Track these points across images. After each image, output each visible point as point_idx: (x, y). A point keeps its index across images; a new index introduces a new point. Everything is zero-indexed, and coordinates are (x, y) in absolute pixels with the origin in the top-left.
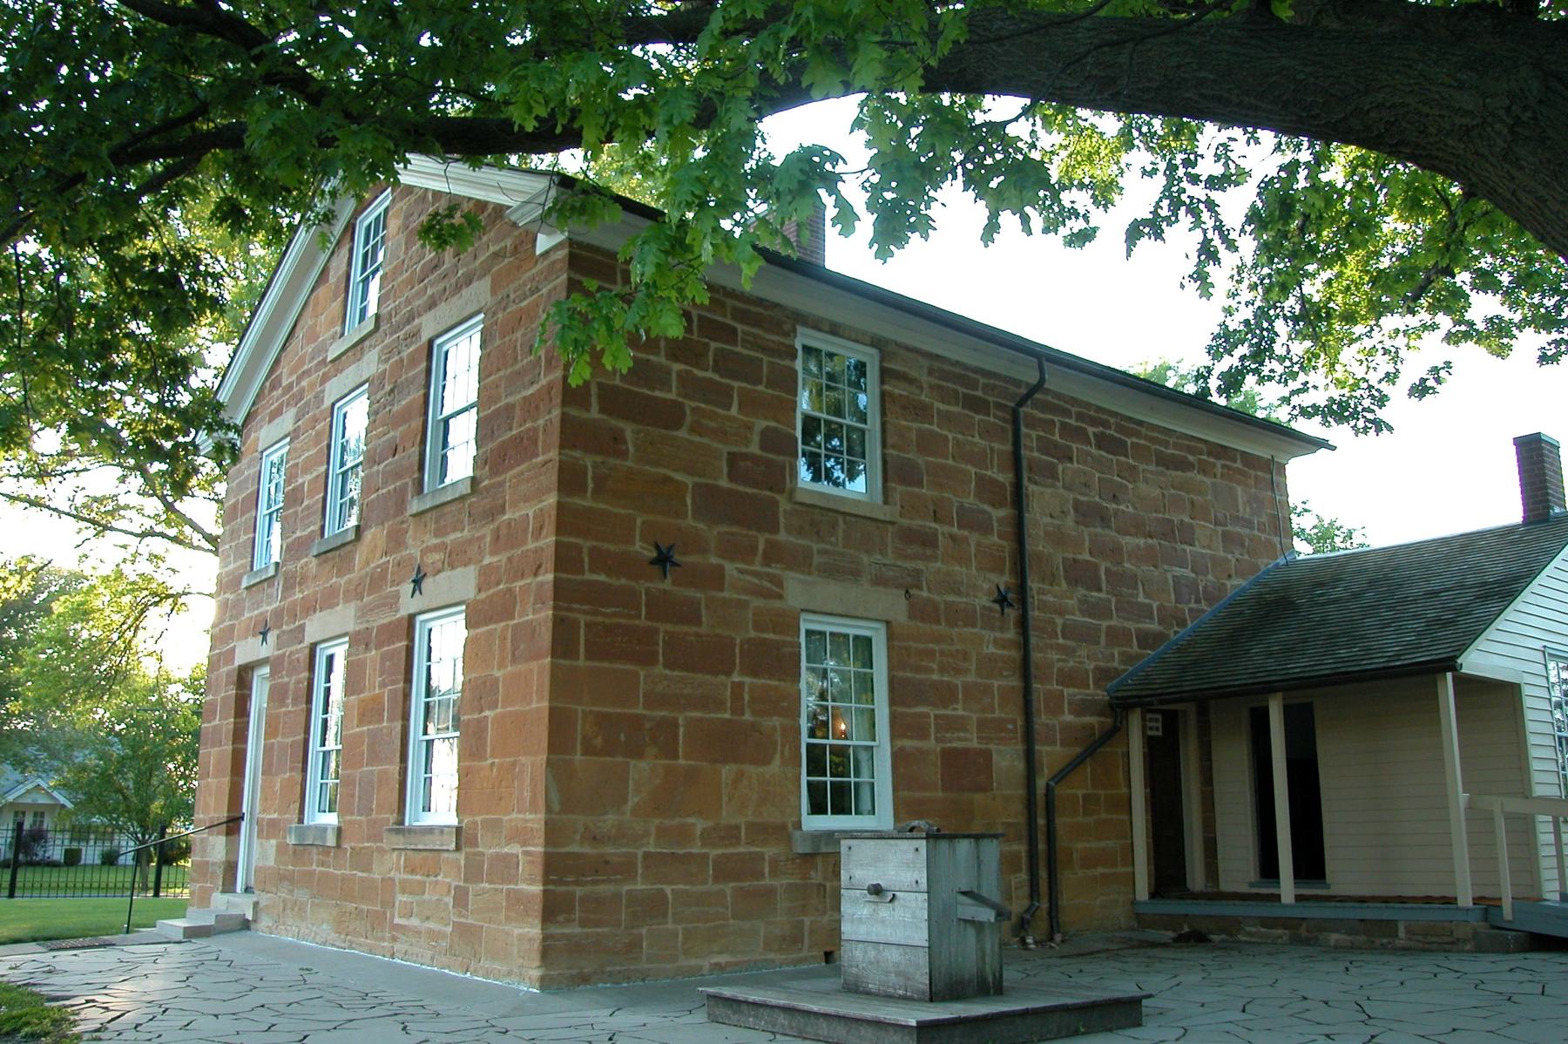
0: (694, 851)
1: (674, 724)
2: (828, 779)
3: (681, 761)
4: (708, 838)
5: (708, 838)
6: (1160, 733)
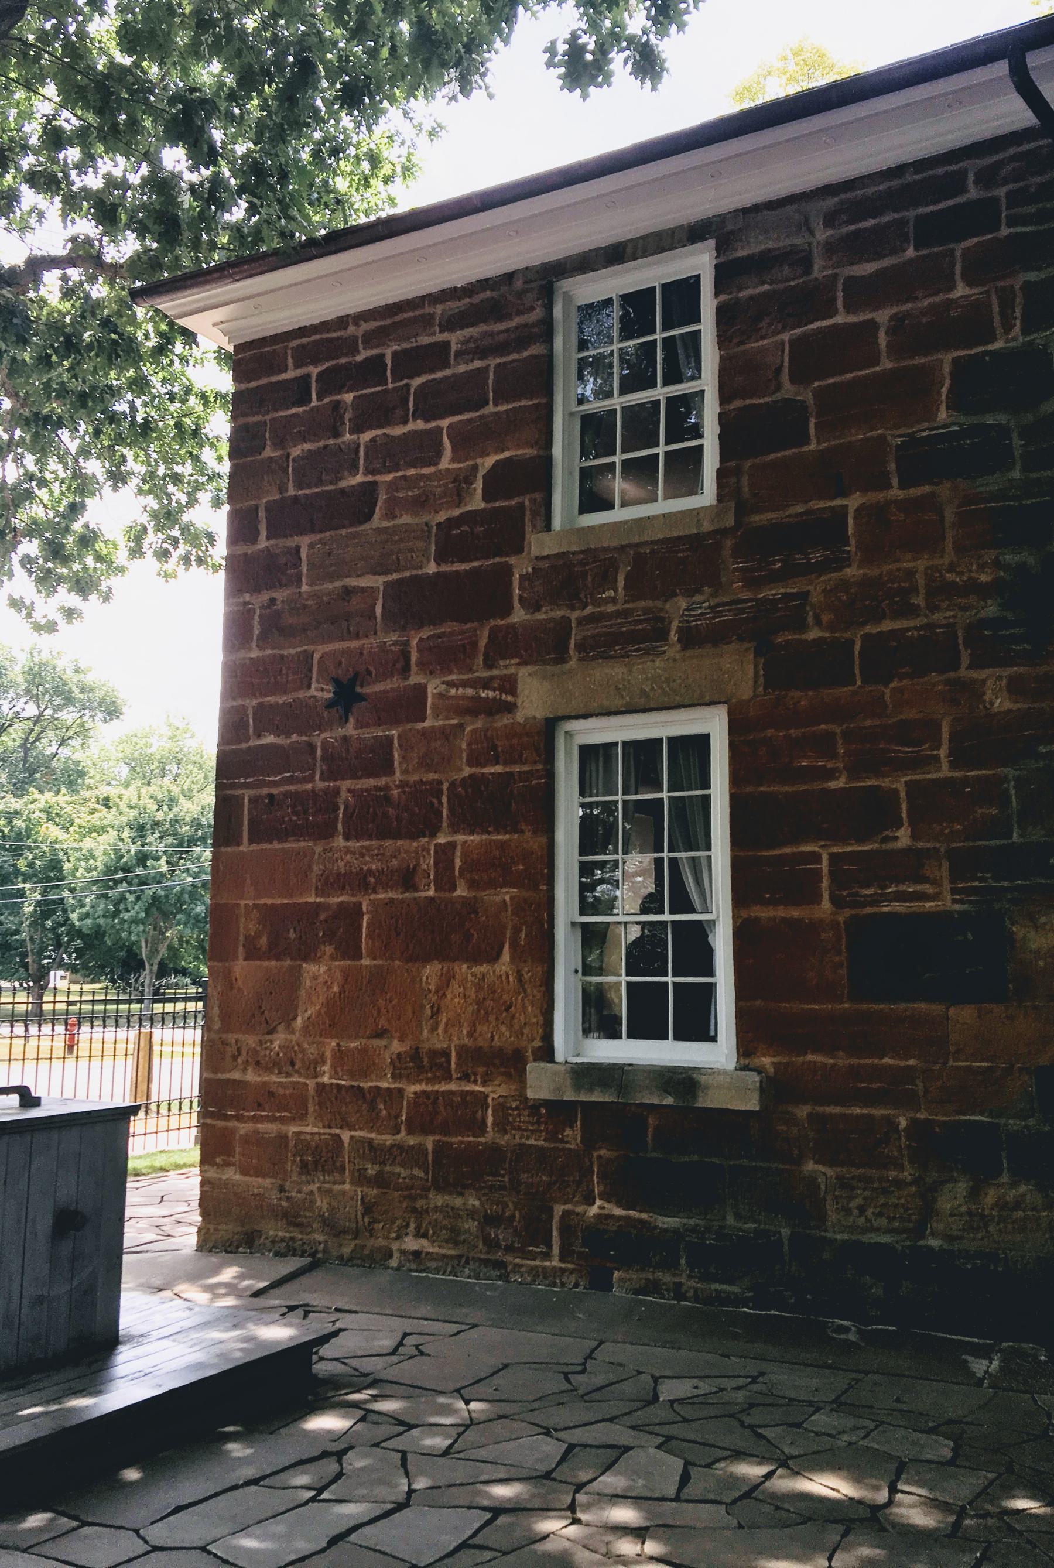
0: (384, 1085)
1: (356, 911)
2: (670, 979)
3: (366, 962)
4: (403, 1067)
5: (403, 1067)
6: (331, 695)
